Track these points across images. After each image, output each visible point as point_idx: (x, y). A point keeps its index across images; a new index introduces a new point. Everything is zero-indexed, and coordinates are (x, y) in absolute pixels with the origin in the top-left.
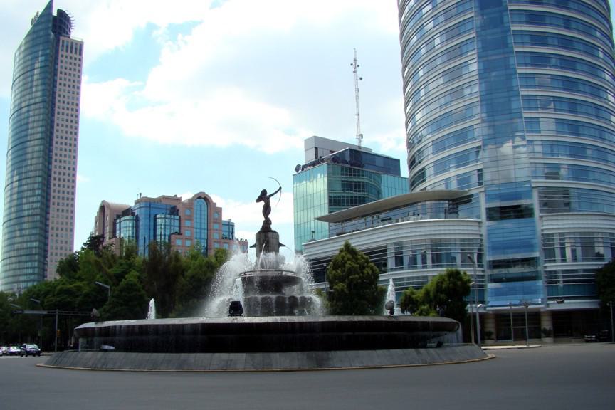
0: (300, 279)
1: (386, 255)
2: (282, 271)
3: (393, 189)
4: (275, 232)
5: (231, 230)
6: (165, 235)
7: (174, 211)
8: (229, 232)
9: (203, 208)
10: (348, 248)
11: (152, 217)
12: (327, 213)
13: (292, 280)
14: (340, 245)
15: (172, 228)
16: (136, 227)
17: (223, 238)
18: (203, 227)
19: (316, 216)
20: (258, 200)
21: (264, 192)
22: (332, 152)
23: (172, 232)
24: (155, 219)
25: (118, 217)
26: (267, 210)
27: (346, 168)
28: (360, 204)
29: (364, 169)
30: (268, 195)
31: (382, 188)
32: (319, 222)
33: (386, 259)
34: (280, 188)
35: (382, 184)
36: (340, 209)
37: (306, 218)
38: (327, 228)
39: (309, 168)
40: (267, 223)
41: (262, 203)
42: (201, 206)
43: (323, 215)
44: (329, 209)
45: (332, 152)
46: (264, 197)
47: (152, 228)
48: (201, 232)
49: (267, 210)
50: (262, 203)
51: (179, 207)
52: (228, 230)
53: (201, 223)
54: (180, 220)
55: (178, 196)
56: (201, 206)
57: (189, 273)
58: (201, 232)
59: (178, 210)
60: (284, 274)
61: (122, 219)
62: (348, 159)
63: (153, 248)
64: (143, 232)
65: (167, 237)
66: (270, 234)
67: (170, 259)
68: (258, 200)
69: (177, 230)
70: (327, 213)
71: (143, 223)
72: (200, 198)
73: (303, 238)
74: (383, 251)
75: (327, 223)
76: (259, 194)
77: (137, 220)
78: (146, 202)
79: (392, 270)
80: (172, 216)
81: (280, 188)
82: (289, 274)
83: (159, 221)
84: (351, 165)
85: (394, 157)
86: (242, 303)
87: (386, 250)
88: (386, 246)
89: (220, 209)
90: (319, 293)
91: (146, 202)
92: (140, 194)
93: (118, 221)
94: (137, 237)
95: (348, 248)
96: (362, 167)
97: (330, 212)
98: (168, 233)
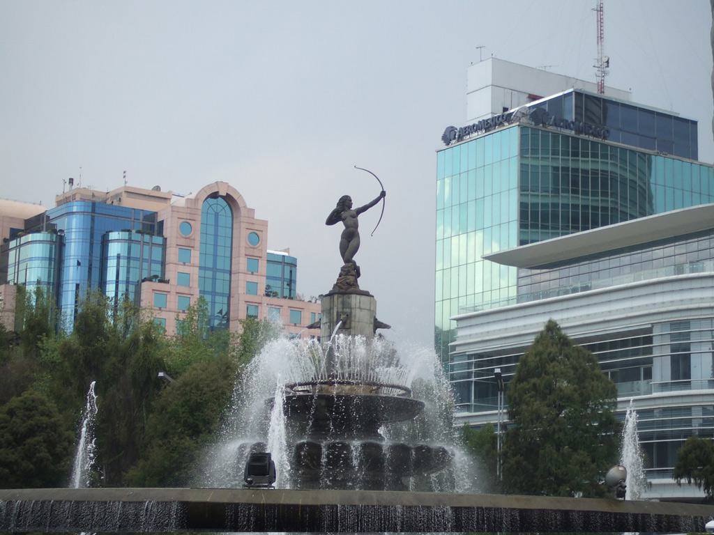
0: (422, 405)
1: (650, 351)
2: (381, 386)
3: (678, 193)
4: (366, 294)
5: (287, 276)
6: (128, 282)
7: (152, 226)
8: (283, 279)
9: (222, 221)
10: (552, 327)
11: (98, 239)
12: (514, 245)
13: (406, 407)
14: (536, 323)
15: (145, 265)
16: (57, 260)
17: (268, 295)
18: (219, 266)
19: (488, 253)
20: (331, 221)
21: (345, 203)
22: (533, 98)
23: (145, 275)
24: (105, 242)
25: (15, 234)
26: (350, 242)
27: (566, 137)
28: (595, 225)
29: (607, 142)
30: (354, 207)
31: (653, 187)
32: (496, 265)
33: (650, 361)
34: (383, 194)
35: (652, 180)
36: (547, 236)
37: (463, 253)
38: (513, 280)
39: (475, 135)
40: (351, 272)
41: (340, 227)
42: (217, 215)
43: (505, 249)
44: (521, 233)
45: (533, 98)
46: (343, 212)
47: (96, 264)
48: (214, 279)
49: (350, 242)
50: (340, 227)
51: (164, 215)
52: (279, 274)
53: (215, 256)
54: (164, 246)
55: (164, 190)
56: (217, 215)
57: (348, 300)
58: (214, 279)
59: (161, 223)
60: (384, 392)
61: (24, 239)
62: (571, 116)
63: (89, 323)
64: (72, 274)
65: (132, 288)
66: (355, 300)
67: (135, 341)
68: (331, 221)
69: (156, 269)
70: (514, 245)
71: (74, 250)
72: (215, 195)
73: (454, 302)
74: (643, 339)
75: (513, 269)
76: (334, 207)
77: (59, 244)
78: (83, 200)
79: (664, 386)
80: (147, 238)
81: (383, 194)
82: (396, 393)
83: (115, 249)
84: (579, 131)
85: (684, 114)
86: (364, 441)
87: (649, 340)
88: (650, 330)
89: (265, 224)
90: (477, 440)
91: (83, 200)
92: (71, 181)
93: (13, 244)
94: (57, 284)
95: (552, 327)
96: (605, 138)
97: (522, 242)
98: (134, 277)
